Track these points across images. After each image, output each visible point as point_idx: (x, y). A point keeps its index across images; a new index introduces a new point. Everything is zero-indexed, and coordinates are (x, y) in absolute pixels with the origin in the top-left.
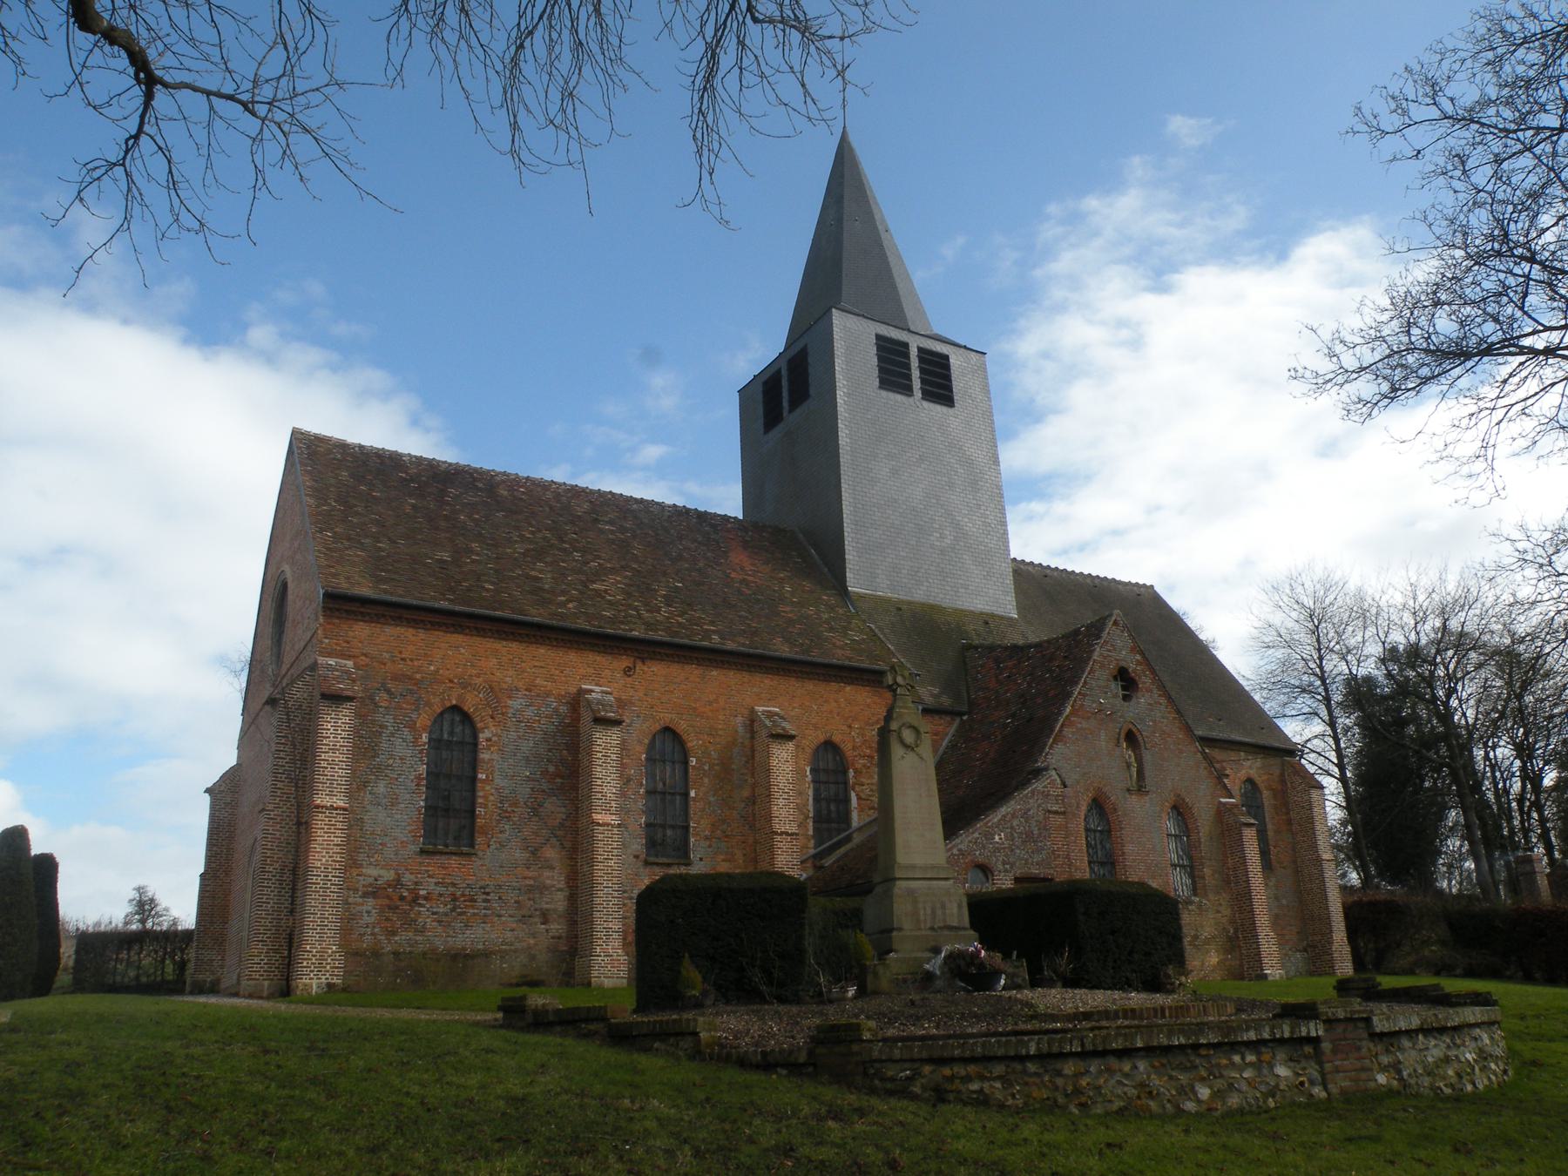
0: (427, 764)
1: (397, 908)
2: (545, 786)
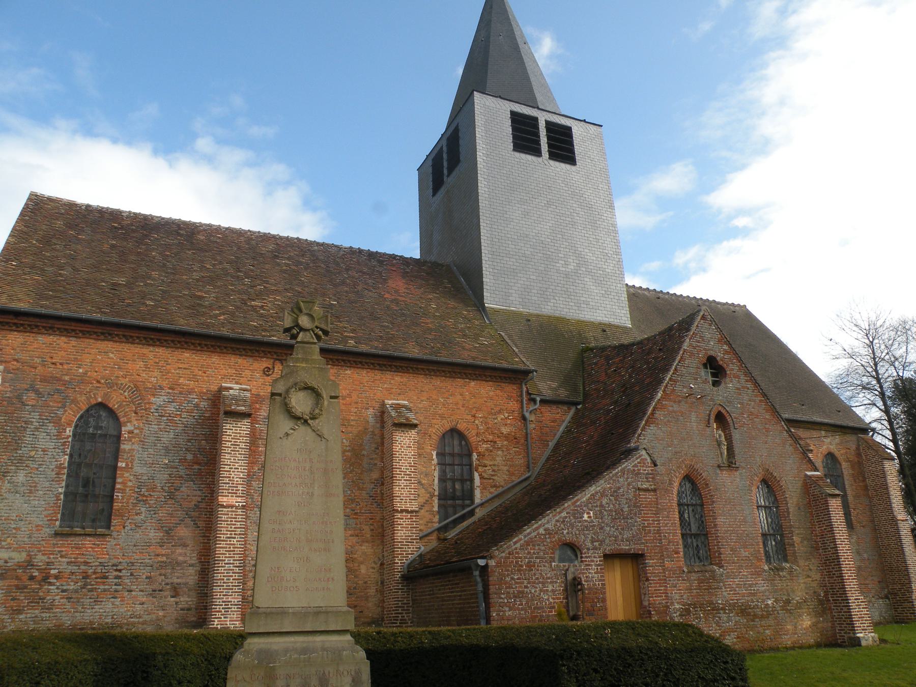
0: (71, 456)
1: (26, 587)
2: (182, 473)
